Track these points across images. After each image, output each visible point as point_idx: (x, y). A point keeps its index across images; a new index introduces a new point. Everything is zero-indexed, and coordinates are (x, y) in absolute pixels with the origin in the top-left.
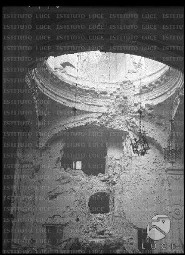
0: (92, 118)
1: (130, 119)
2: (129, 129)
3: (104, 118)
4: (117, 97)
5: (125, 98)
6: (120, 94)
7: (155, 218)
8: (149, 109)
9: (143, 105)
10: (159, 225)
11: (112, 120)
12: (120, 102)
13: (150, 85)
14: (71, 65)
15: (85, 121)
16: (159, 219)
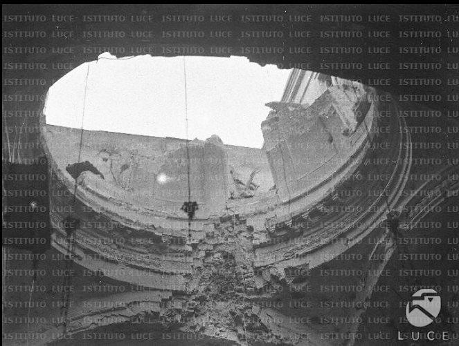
0: (147, 305)
1: (246, 308)
2: (239, 336)
3: (178, 305)
4: (208, 254)
5: (227, 256)
6: (215, 246)
7: (418, 294)
8: (294, 282)
9: (280, 271)
10: (424, 304)
11: (196, 312)
12: (216, 266)
13: (297, 219)
14: (95, 171)
15: (129, 312)
16: (424, 295)
